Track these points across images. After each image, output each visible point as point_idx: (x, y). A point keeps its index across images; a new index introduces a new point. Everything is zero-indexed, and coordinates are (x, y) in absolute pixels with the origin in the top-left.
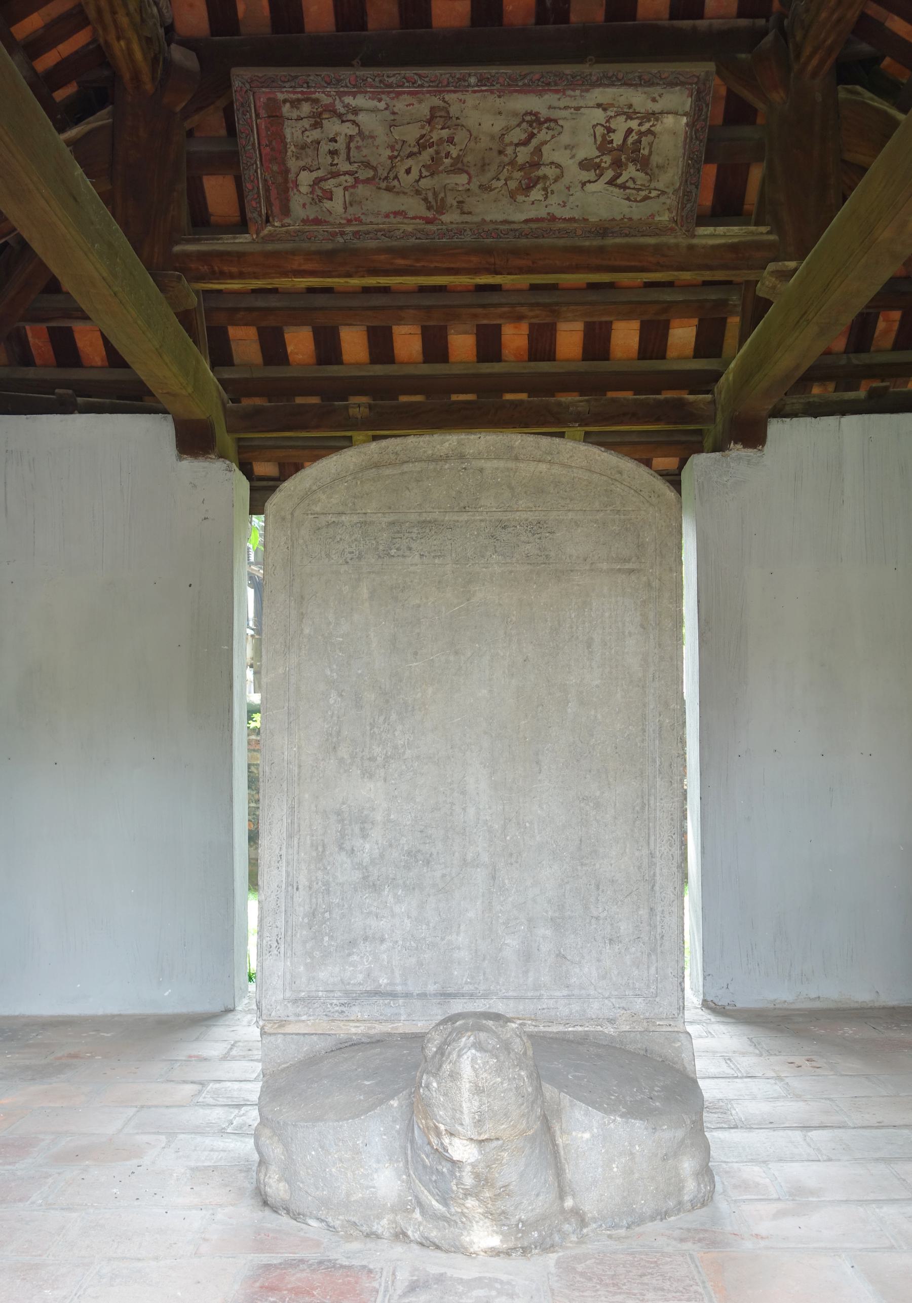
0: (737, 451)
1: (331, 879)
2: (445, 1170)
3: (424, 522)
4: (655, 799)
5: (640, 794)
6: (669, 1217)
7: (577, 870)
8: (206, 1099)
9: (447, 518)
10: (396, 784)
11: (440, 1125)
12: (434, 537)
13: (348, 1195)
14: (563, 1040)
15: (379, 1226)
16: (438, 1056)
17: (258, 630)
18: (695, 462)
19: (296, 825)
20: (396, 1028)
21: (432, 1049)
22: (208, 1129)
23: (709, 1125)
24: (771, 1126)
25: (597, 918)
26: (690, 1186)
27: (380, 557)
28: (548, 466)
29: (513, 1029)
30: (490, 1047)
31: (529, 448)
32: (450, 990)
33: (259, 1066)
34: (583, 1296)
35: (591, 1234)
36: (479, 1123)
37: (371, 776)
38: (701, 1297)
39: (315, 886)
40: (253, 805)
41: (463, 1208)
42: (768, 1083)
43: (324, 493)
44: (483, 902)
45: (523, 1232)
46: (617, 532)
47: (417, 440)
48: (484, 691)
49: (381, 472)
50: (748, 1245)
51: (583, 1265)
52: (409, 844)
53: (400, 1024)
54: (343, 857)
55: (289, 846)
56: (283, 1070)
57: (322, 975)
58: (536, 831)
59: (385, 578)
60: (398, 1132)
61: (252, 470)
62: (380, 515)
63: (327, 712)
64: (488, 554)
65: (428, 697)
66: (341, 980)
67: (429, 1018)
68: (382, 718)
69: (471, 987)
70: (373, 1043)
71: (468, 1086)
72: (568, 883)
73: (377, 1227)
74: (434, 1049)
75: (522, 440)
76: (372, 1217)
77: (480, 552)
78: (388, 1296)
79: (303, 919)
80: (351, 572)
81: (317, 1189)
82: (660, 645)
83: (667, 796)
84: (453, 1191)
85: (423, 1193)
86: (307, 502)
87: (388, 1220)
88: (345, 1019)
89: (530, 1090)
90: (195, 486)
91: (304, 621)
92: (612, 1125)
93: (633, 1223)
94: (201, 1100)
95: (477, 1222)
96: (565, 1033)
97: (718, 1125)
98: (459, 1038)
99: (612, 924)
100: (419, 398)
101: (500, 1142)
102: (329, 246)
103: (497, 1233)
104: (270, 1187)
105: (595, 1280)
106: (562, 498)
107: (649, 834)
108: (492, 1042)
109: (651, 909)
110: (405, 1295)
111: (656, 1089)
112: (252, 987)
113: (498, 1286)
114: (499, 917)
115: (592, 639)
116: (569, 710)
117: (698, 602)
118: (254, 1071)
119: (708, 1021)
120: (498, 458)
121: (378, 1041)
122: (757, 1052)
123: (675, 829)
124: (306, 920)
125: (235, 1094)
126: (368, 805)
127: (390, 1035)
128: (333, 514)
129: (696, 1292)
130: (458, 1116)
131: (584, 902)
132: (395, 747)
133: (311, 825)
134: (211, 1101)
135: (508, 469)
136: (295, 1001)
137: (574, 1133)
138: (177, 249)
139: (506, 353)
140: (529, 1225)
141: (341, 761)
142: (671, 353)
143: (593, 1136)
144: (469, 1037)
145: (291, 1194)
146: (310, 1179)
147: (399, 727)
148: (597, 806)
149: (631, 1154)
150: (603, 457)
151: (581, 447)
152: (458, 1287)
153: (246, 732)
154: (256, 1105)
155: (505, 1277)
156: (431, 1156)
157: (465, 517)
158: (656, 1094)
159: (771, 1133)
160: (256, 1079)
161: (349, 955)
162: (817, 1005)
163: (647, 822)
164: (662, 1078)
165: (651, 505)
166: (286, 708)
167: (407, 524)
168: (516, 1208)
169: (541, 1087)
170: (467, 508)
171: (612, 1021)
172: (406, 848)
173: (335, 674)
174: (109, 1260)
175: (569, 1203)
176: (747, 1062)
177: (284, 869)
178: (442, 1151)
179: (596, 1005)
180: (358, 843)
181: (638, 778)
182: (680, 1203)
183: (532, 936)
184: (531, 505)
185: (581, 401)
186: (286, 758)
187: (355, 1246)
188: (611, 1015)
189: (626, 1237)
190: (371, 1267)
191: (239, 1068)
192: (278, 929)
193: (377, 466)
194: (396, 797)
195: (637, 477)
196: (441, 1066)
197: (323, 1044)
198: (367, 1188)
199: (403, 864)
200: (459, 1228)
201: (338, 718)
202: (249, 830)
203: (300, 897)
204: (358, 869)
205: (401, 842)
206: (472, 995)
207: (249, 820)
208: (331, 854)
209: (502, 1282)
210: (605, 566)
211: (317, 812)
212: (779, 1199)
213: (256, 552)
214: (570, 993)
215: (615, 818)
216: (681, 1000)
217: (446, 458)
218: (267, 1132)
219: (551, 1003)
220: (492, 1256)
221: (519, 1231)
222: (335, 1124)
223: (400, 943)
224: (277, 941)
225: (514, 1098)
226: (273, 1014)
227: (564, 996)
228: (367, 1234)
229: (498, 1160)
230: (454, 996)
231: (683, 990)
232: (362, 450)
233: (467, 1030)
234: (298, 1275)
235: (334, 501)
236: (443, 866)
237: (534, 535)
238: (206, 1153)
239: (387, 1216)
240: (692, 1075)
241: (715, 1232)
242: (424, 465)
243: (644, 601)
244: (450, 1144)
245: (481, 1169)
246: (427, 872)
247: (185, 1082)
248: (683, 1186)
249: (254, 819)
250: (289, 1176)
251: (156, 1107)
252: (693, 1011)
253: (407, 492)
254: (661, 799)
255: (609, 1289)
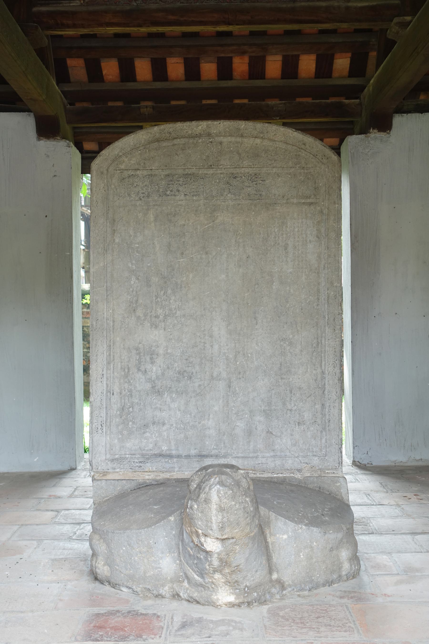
0: (374, 134)
1: (133, 388)
2: (202, 557)
3: (186, 174)
4: (325, 339)
5: (316, 337)
6: (334, 584)
7: (279, 382)
8: (60, 520)
9: (200, 172)
10: (171, 331)
11: (199, 530)
12: (193, 184)
13: (145, 573)
14: (271, 482)
15: (163, 590)
16: (197, 490)
17: (88, 246)
18: (349, 140)
19: (112, 356)
20: (172, 476)
21: (194, 485)
22: (62, 537)
23: (357, 532)
24: (394, 532)
25: (291, 410)
26: (346, 566)
27: (160, 196)
28: (261, 141)
29: (241, 474)
30: (228, 484)
31: (249, 130)
32: (204, 453)
33: (91, 501)
34: (283, 630)
35: (288, 594)
36: (222, 529)
37: (156, 327)
38: (352, 630)
39: (124, 393)
40: (85, 350)
41: (213, 579)
42: (391, 508)
43: (126, 157)
44: (223, 401)
45: (248, 593)
46: (302, 180)
47: (182, 125)
48: (223, 276)
49: (160, 144)
50: (380, 600)
51: (283, 612)
52: (179, 367)
53: (174, 474)
54: (140, 375)
55: (108, 369)
56: (107, 500)
57: (128, 445)
58: (254, 359)
59: (164, 208)
60: (174, 535)
61: (82, 146)
62: (160, 170)
63: (130, 289)
64: (225, 193)
65: (190, 279)
66: (140, 447)
67: (191, 470)
68: (162, 293)
69: (217, 451)
70: (158, 484)
71: (215, 507)
72: (273, 389)
73: (162, 591)
74: (195, 486)
75: (245, 125)
76: (159, 586)
77: (221, 192)
78: (169, 631)
79: (117, 412)
80: (143, 205)
81: (127, 569)
82: (328, 248)
83: (332, 338)
84: (207, 570)
85: (189, 571)
86: (116, 163)
87: (168, 587)
88: (142, 470)
89: (252, 509)
90: (48, 156)
91: (115, 234)
92: (300, 530)
93: (313, 588)
94: (57, 520)
95: (221, 587)
96: (272, 478)
97: (362, 532)
98: (210, 479)
99: (299, 414)
100: (183, 102)
101: (234, 540)
102: (128, 8)
103: (233, 594)
104: (99, 569)
105: (290, 621)
106: (270, 160)
107: (321, 360)
108: (230, 481)
109: (323, 405)
110: (179, 630)
111: (326, 510)
112: (87, 456)
113: (234, 624)
114: (232, 410)
115: (287, 244)
116: (274, 287)
117: (351, 225)
118: (88, 504)
119: (356, 473)
120: (231, 136)
121: (162, 483)
122: (385, 490)
123: (337, 357)
124: (118, 413)
125: (77, 517)
126: (154, 344)
127: (168, 479)
128: (132, 170)
129: (349, 627)
130: (209, 524)
131: (283, 400)
132: (171, 310)
133: (121, 356)
134: (63, 521)
135: (237, 143)
136: (112, 460)
137: (278, 535)
138: (35, 9)
139: (236, 74)
140: (250, 589)
141: (138, 318)
142: (335, 74)
143: (289, 537)
144: (216, 478)
145: (111, 572)
146: (122, 564)
147: (173, 298)
148: (291, 344)
149: (311, 547)
150: (294, 135)
151: (281, 128)
152: (210, 625)
153: (81, 306)
154: (90, 523)
155: (237, 619)
156: (194, 549)
157: (211, 172)
158: (326, 512)
159: (393, 536)
160: (89, 508)
161: (144, 433)
162: (420, 464)
163: (320, 353)
164: (329, 504)
165: (323, 163)
166: (105, 287)
167: (177, 176)
168: (244, 579)
169: (258, 508)
170: (213, 166)
171: (299, 471)
172: (177, 370)
173: (134, 266)
174: (4, 612)
175: (275, 576)
176: (379, 496)
177: (105, 382)
178: (200, 545)
179: (290, 462)
180: (149, 366)
181: (315, 327)
182: (340, 576)
183: (252, 421)
184: (251, 164)
185: (281, 104)
186: (105, 316)
187: (149, 602)
188: (299, 467)
189: (309, 596)
190: (159, 614)
191: (79, 502)
192: (102, 418)
193: (158, 140)
194: (171, 339)
195: (314, 147)
196: (199, 495)
197: (129, 486)
198: (156, 568)
199: (175, 379)
200: (211, 591)
201: (136, 292)
202: (84, 366)
203: (115, 399)
204: (149, 382)
205: (175, 366)
206: (217, 456)
207: (84, 360)
208: (133, 373)
209: (236, 622)
210: (295, 201)
211: (124, 348)
212: (398, 574)
213: (85, 198)
214: (275, 454)
215: (301, 351)
216: (340, 458)
217: (200, 136)
218: (97, 537)
219: (264, 460)
220: (230, 607)
221: (246, 592)
222: (137, 531)
223: (174, 425)
224: (101, 425)
225: (242, 514)
226: (99, 468)
227: (271, 456)
228: (156, 595)
229: (233, 550)
230: (206, 456)
231: (341, 452)
232: (149, 131)
233: (214, 474)
234: (116, 619)
235: (132, 162)
236: (199, 380)
237: (252, 182)
238: (61, 551)
239: (168, 585)
240: (347, 502)
241: (360, 593)
242: (186, 140)
243: (319, 222)
244: (205, 541)
245: (223, 556)
246: (190, 383)
247: (47, 510)
248: (342, 567)
249: (86, 358)
250: (110, 562)
251: (31, 525)
252: (347, 467)
253: (177, 157)
254: (329, 340)
255: (298, 626)
